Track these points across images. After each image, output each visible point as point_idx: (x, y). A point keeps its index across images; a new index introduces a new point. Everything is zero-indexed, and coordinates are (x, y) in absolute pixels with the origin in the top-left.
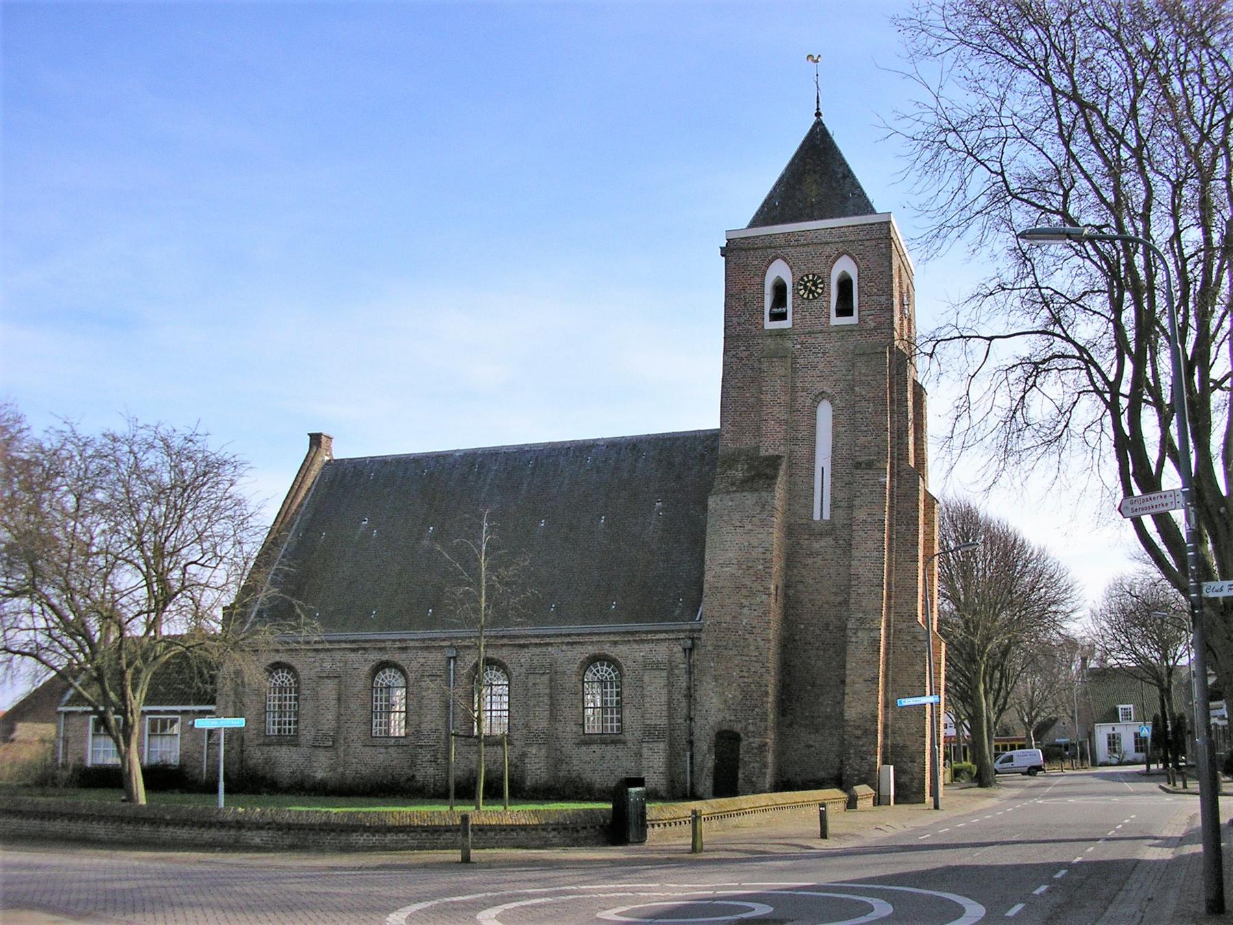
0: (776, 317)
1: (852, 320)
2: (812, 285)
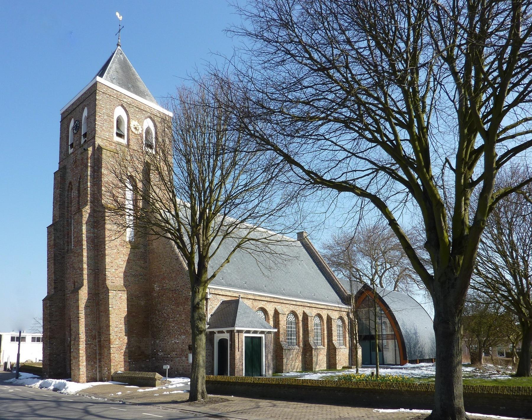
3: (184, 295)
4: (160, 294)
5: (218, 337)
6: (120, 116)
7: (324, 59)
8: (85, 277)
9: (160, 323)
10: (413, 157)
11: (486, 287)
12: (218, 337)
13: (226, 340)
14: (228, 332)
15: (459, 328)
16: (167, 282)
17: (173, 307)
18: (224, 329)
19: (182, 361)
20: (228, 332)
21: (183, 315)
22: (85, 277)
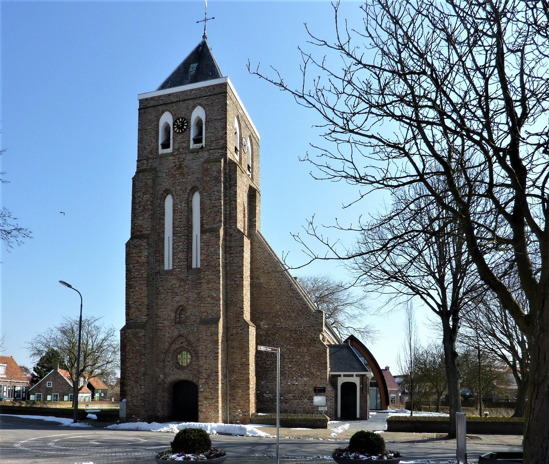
0: (166, 145)
1: (170, 150)
2: (182, 125)
3: (309, 336)
4: (269, 332)
5: (341, 381)
6: (198, 117)
7: (517, 83)
8: (221, 314)
9: (268, 363)
10: (519, 116)
11: (473, 286)
12: (341, 381)
13: (353, 385)
14: (357, 376)
15: (416, 386)
16: (282, 320)
17: (291, 347)
18: (355, 373)
19: (302, 404)
20: (357, 376)
21: (306, 357)
22: (221, 314)
